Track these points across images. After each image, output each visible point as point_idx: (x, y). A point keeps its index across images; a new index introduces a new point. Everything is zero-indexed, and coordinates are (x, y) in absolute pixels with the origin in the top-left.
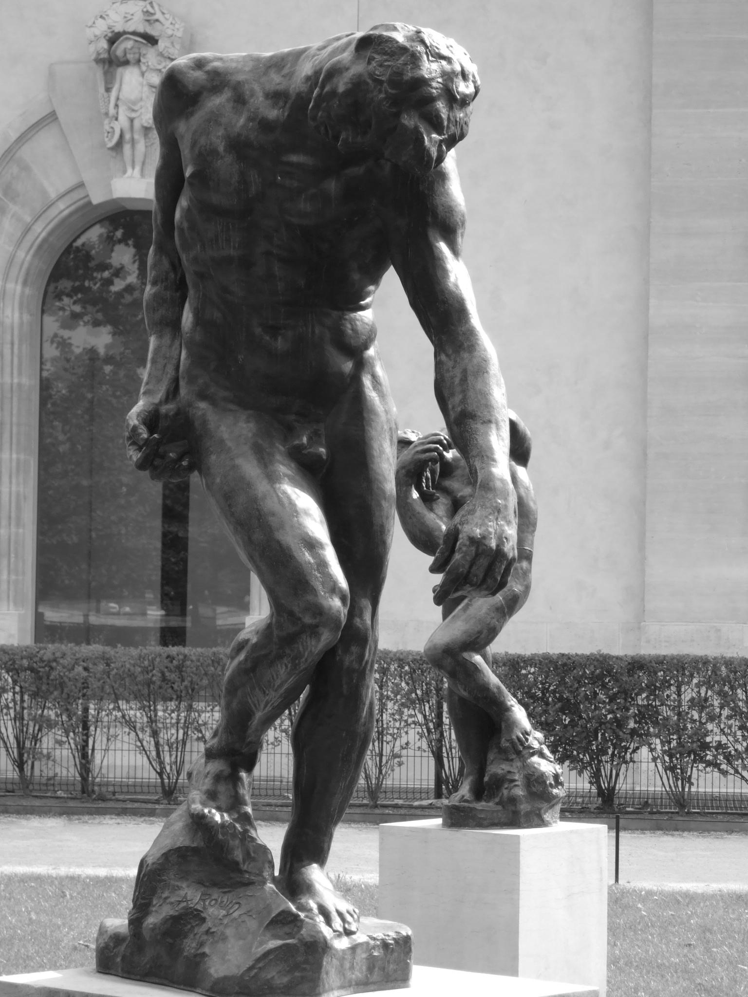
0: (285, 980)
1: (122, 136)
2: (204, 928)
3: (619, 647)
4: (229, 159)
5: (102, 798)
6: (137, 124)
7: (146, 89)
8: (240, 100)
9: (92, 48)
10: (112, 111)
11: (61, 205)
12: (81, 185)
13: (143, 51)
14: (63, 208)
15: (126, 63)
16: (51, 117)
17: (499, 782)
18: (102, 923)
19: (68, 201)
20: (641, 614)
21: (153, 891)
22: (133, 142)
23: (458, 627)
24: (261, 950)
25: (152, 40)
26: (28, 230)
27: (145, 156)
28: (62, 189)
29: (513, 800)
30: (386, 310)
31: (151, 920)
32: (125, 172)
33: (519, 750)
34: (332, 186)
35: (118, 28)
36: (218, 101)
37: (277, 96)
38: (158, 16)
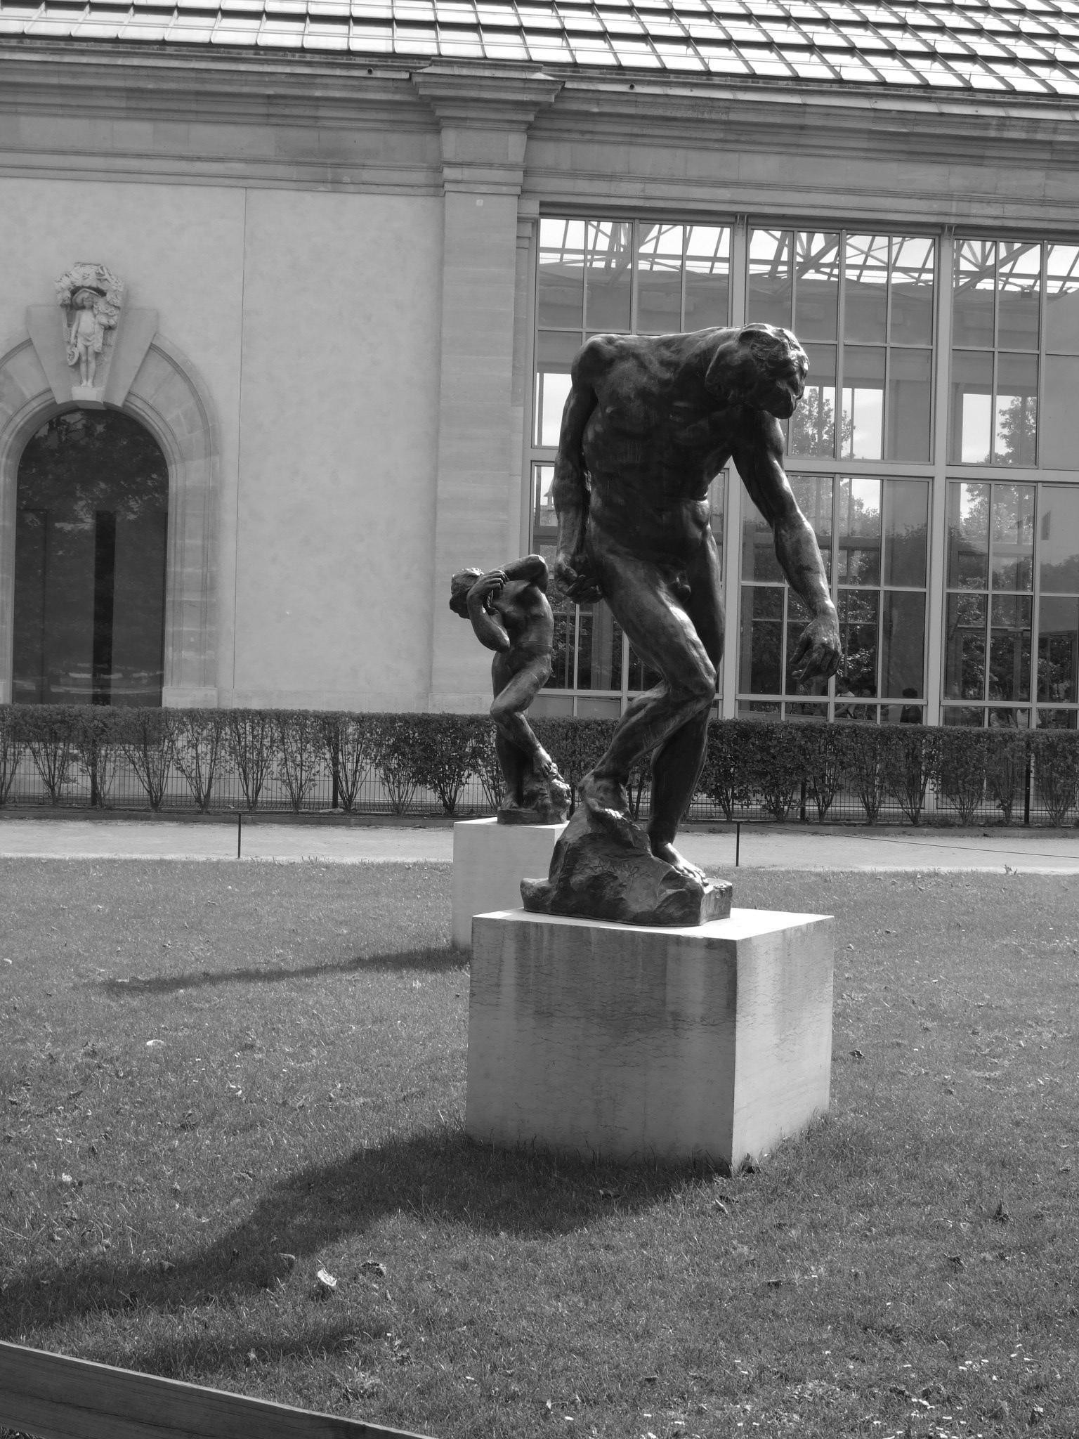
0: (680, 913)
1: (79, 358)
2: (617, 883)
3: (416, 708)
4: (638, 402)
5: (110, 809)
6: (90, 350)
7: (97, 326)
8: (642, 366)
9: (59, 296)
10: (73, 340)
11: (34, 404)
12: (49, 390)
13: (95, 300)
14: (35, 406)
15: (83, 308)
16: (28, 343)
17: (534, 796)
18: (523, 885)
19: (39, 401)
20: (429, 689)
21: (576, 861)
22: (87, 362)
23: (510, 696)
24: (663, 896)
25: (102, 293)
26: (10, 420)
27: (96, 372)
28: (36, 393)
29: (545, 807)
30: (726, 498)
31: (578, 879)
32: (81, 383)
33: (546, 775)
34: (703, 423)
35: (79, 284)
36: (628, 366)
37: (665, 364)
38: (107, 276)
